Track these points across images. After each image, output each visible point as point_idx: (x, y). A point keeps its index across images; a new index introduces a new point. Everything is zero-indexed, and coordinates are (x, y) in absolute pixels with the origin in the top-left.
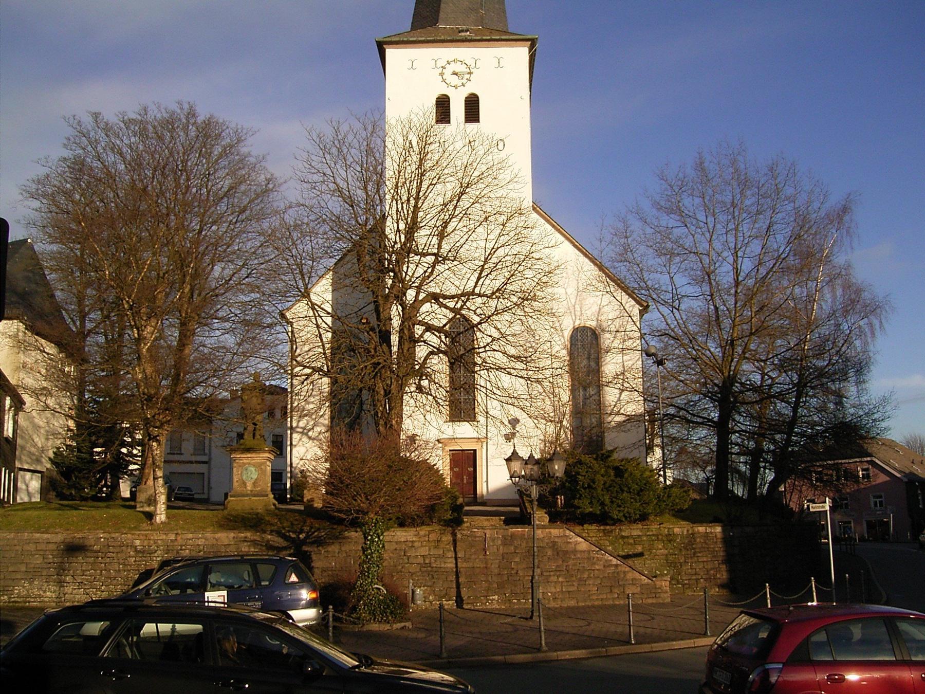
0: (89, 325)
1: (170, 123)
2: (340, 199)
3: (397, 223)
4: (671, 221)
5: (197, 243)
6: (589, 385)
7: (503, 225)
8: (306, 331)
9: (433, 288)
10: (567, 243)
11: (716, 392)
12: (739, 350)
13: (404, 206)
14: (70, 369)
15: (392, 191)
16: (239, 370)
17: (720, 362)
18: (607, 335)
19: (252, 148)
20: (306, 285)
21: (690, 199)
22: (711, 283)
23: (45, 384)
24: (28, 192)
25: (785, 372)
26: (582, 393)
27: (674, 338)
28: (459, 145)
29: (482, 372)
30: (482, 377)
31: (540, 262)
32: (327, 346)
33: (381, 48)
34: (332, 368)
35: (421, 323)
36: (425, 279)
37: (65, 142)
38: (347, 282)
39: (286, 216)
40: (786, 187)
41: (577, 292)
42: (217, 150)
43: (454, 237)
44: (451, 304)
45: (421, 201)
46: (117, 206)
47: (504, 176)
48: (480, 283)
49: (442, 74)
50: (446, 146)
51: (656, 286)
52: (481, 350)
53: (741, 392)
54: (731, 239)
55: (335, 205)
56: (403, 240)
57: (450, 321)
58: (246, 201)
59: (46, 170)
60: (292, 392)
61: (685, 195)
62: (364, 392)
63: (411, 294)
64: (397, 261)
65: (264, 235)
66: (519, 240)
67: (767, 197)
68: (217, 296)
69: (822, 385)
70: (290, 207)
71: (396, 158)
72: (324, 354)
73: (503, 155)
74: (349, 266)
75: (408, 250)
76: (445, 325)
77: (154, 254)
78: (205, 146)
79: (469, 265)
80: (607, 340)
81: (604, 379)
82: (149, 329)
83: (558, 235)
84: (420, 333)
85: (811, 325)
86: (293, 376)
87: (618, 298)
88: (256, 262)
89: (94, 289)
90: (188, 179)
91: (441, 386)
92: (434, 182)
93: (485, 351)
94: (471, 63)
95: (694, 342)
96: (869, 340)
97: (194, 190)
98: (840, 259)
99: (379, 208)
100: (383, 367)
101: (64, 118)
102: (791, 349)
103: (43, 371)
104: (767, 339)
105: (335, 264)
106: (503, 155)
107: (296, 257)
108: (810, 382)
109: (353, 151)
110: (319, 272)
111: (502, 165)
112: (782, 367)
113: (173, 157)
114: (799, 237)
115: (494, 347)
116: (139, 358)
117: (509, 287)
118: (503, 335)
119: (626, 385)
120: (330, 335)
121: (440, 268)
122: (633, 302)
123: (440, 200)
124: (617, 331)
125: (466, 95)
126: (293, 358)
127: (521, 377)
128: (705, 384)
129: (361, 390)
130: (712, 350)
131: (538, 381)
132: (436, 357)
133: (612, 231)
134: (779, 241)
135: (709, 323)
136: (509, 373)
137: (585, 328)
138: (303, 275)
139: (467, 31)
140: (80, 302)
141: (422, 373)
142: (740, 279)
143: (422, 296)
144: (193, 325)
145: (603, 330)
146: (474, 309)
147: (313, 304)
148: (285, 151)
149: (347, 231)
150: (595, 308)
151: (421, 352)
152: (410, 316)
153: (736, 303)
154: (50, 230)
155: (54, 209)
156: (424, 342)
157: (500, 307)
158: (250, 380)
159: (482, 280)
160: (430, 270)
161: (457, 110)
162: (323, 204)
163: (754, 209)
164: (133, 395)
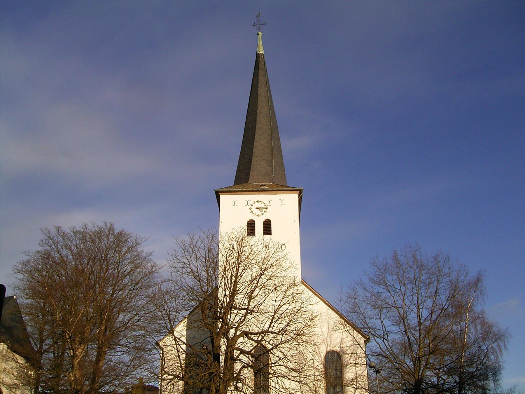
0: (45, 347)
1: (99, 234)
2: (193, 277)
3: (225, 291)
4: (381, 289)
5: (110, 301)
6: (336, 386)
7: (285, 292)
8: (170, 353)
9: (245, 329)
10: (321, 302)
11: (411, 389)
12: (423, 363)
13: (229, 281)
14: (31, 373)
15: (222, 273)
16: (130, 376)
17: (413, 371)
18: (346, 356)
19: (145, 249)
20: (172, 326)
21: (390, 276)
22: (405, 324)
23: (16, 381)
24: (17, 269)
25: (451, 375)
26: (332, 390)
27: (385, 357)
28: (260, 247)
29: (273, 378)
30: (273, 382)
31: (306, 313)
32: (183, 362)
33: (218, 194)
34: (185, 375)
35: (238, 349)
36: (240, 323)
37: (40, 242)
38: (196, 324)
39: (162, 286)
40: (444, 269)
41: (328, 331)
42: (125, 249)
43: (257, 299)
44: (255, 338)
45: (238, 279)
46: (66, 279)
47: (285, 265)
48: (272, 325)
49: (251, 209)
50: (253, 247)
51: (374, 326)
52: (273, 365)
53: (426, 388)
54: (415, 298)
55: (190, 281)
56: (228, 301)
57: (254, 348)
58: (139, 277)
59: (28, 258)
60: (161, 389)
61: (387, 274)
62: (204, 390)
63: (232, 332)
64: (224, 313)
65: (149, 297)
66: (294, 301)
67: (434, 274)
68: (120, 332)
69: (473, 383)
70: (164, 281)
71: (225, 254)
72: (181, 367)
73: (284, 253)
74: (197, 315)
75: (231, 306)
76: (252, 350)
77: (86, 307)
78: (118, 247)
79: (266, 315)
80: (346, 358)
81: (345, 382)
82: (80, 350)
83: (316, 298)
84: (237, 355)
85: (464, 347)
86: (162, 380)
87: (352, 334)
88: (144, 312)
89: (50, 326)
90: (108, 265)
91: (249, 387)
92: (246, 268)
93: (275, 366)
94: (267, 202)
95: (397, 359)
96: (499, 355)
97: (111, 271)
98: (478, 309)
99: (214, 282)
100: (215, 375)
101: (41, 229)
102: (453, 362)
103: (16, 374)
104: (439, 356)
105: (189, 314)
106: (284, 253)
107: (167, 310)
108: (466, 381)
109: (201, 251)
110: (179, 319)
111: (284, 258)
112: (449, 373)
113: (100, 252)
114: (453, 296)
115: (280, 363)
116: (73, 367)
117: (289, 328)
118: (286, 356)
119: (358, 385)
120: (184, 356)
121: (249, 317)
122: (360, 336)
123: (249, 278)
124: (352, 353)
125: (264, 220)
126: (163, 369)
127: (297, 381)
128: (405, 384)
129: (202, 389)
130: (408, 363)
131: (306, 384)
132: (246, 369)
133: (347, 295)
134: (443, 299)
135: (405, 348)
136: (289, 379)
137: (333, 352)
138: (170, 321)
139: (264, 185)
140: (41, 333)
141: (238, 379)
142: (422, 321)
143: (238, 333)
144: (105, 349)
145: (344, 353)
146: (269, 341)
147: (175, 338)
148: (161, 252)
149: (196, 296)
150: (339, 340)
151: (238, 366)
152: (231, 345)
153: (420, 336)
154: (27, 291)
155: (31, 279)
156: (240, 360)
157: (283, 339)
158: (137, 382)
159: (273, 324)
160: (243, 318)
161: (259, 228)
162: (183, 280)
163: (427, 281)
164: (67, 390)
